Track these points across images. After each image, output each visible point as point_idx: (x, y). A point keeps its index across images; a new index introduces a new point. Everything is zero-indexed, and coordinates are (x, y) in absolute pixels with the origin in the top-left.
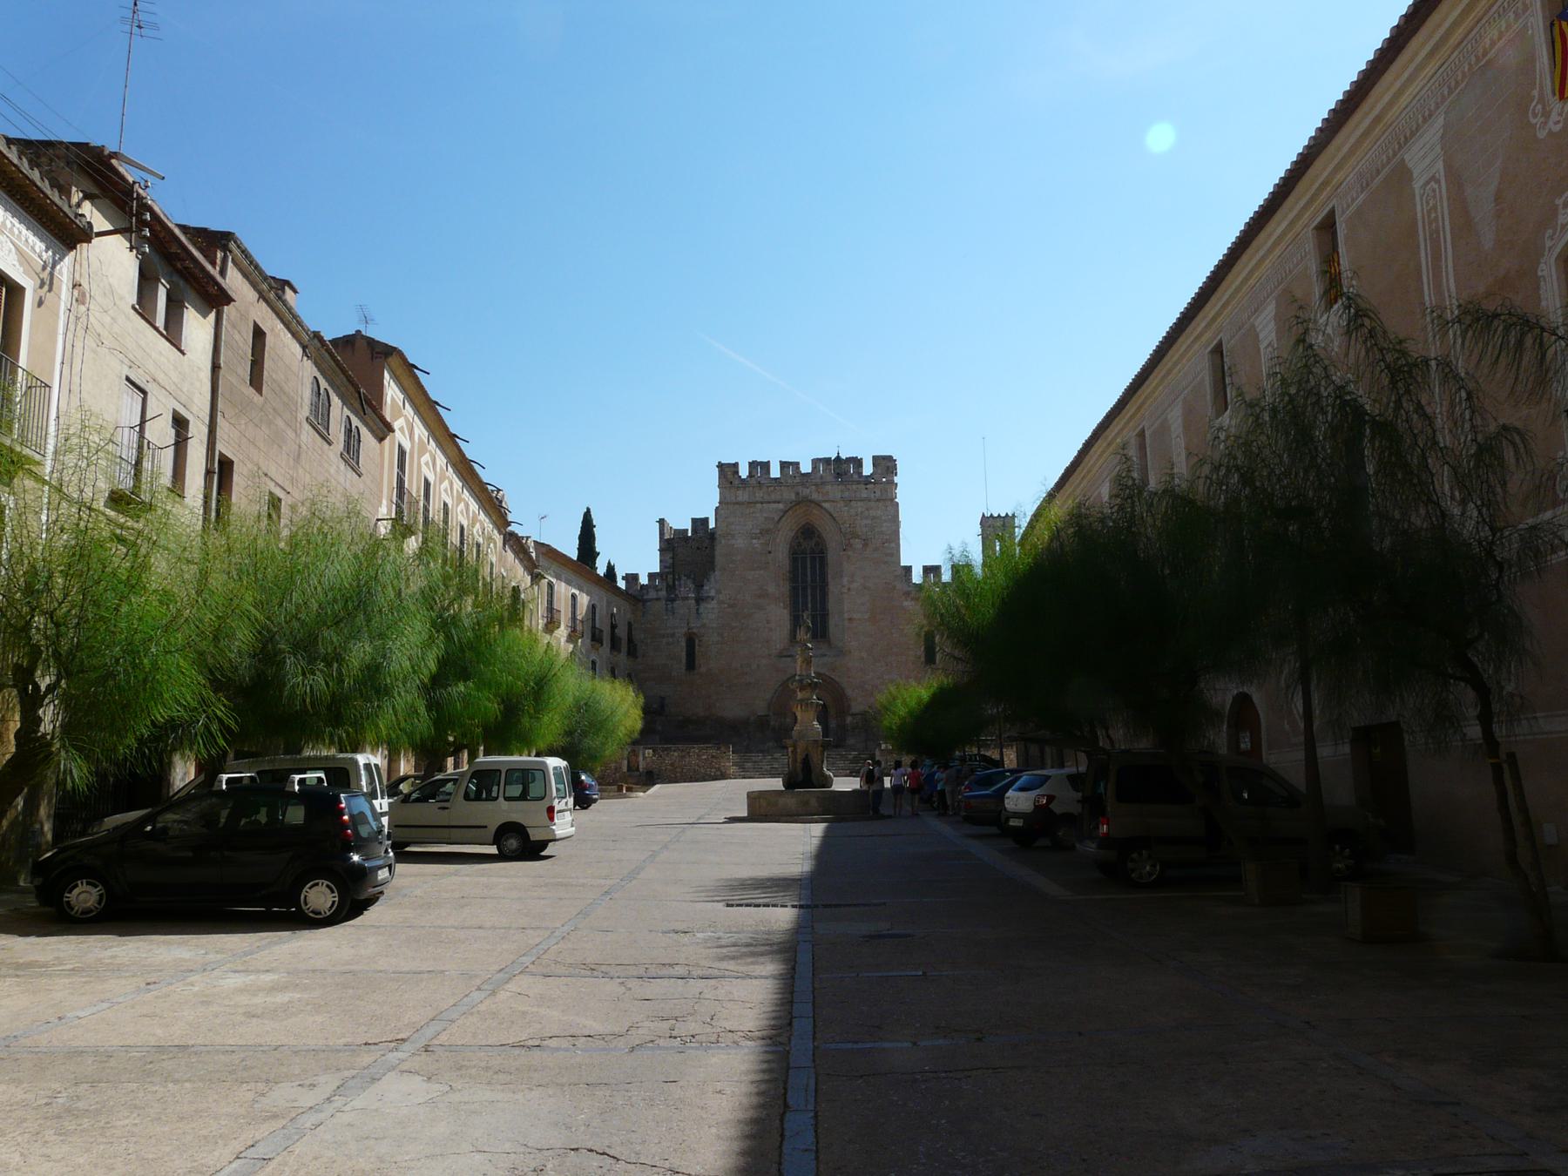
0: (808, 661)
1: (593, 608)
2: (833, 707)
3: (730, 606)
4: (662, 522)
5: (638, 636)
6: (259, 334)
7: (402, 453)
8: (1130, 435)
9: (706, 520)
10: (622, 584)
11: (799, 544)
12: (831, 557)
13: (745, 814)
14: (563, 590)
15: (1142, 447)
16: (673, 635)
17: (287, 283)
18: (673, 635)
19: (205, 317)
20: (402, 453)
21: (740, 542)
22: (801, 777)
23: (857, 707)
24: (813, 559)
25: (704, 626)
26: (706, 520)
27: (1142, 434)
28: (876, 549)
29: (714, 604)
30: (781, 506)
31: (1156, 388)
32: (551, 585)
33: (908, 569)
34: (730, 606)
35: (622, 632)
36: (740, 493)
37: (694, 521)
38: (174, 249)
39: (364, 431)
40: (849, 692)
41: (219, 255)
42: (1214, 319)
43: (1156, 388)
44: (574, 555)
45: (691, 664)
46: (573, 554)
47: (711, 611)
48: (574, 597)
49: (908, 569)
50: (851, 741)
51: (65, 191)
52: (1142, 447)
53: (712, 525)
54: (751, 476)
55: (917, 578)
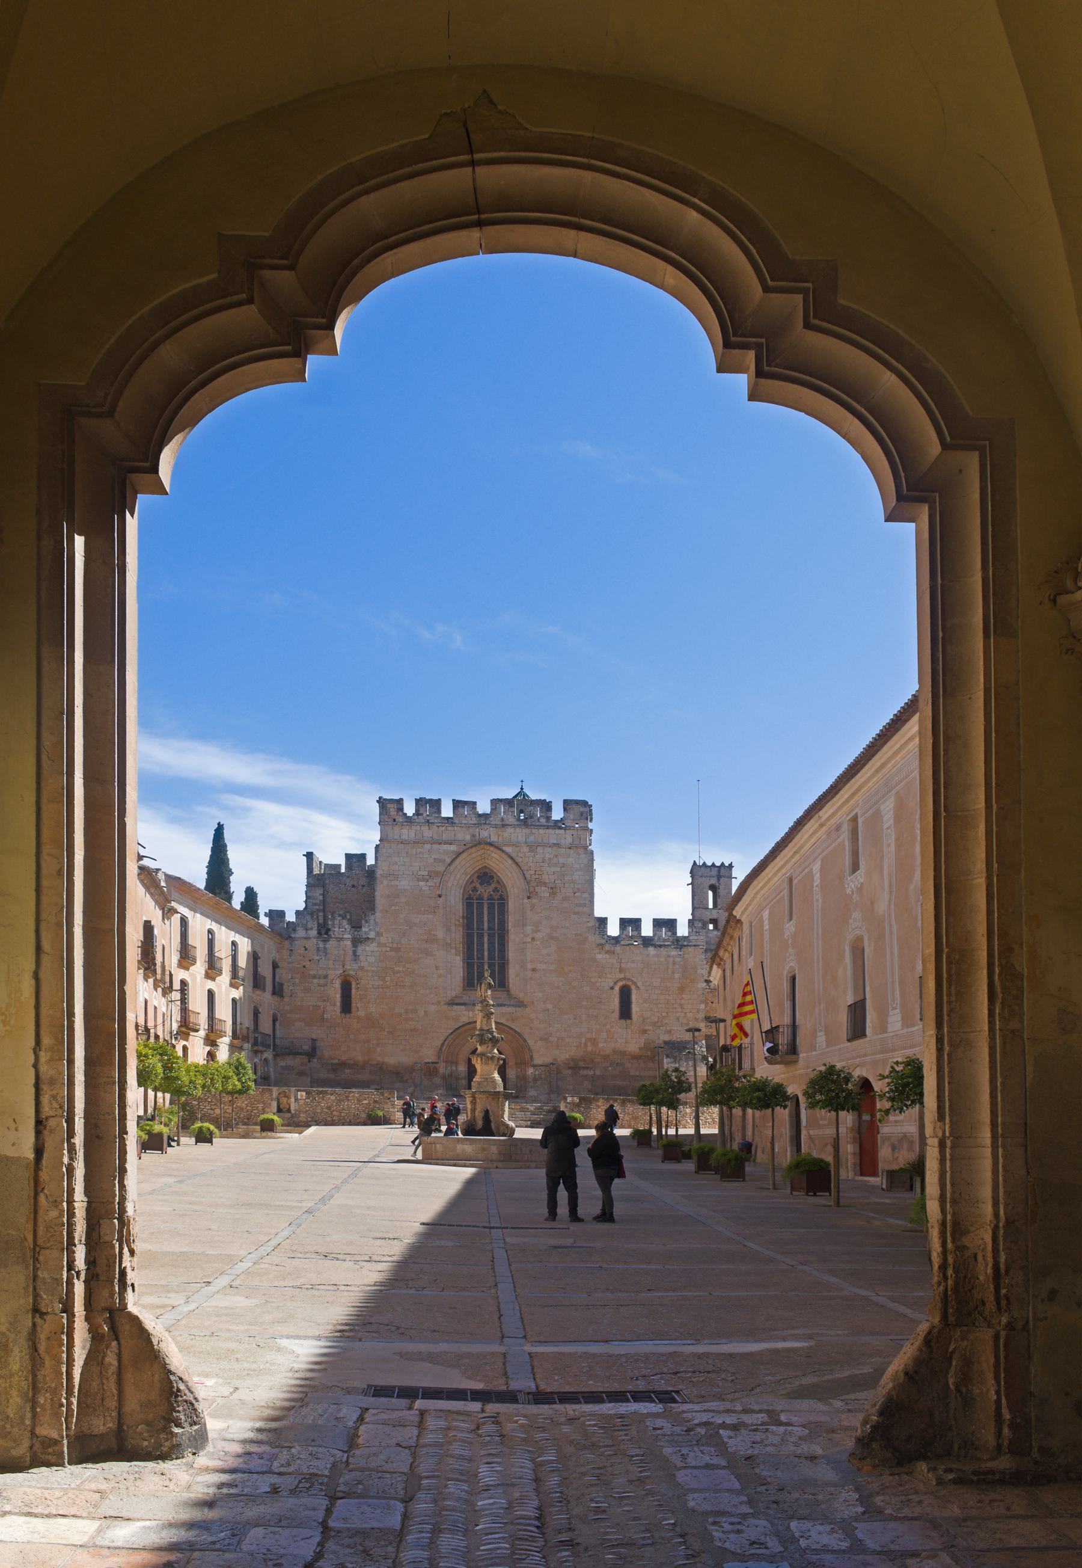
0: (488, 1016)
2: (515, 1058)
3: (392, 949)
4: (309, 856)
5: (283, 974)
8: (843, 817)
9: (362, 857)
10: (264, 921)
11: (475, 890)
12: (512, 905)
14: (200, 924)
15: (854, 833)
16: (326, 977)
18: (326, 977)
21: (404, 884)
22: (480, 1124)
23: (542, 1056)
24: (491, 907)
25: (362, 968)
26: (362, 857)
27: (855, 819)
28: (565, 899)
29: (371, 947)
30: (453, 848)
31: (869, 779)
32: (184, 922)
33: (603, 922)
34: (392, 949)
35: (265, 970)
36: (405, 831)
37: (349, 857)
40: (531, 1043)
42: (883, 766)
43: (869, 779)
44: (201, 884)
45: (347, 1006)
46: (199, 877)
47: (368, 951)
49: (603, 922)
50: (532, 1093)
52: (854, 833)
53: (370, 861)
54: (418, 813)
55: (613, 930)
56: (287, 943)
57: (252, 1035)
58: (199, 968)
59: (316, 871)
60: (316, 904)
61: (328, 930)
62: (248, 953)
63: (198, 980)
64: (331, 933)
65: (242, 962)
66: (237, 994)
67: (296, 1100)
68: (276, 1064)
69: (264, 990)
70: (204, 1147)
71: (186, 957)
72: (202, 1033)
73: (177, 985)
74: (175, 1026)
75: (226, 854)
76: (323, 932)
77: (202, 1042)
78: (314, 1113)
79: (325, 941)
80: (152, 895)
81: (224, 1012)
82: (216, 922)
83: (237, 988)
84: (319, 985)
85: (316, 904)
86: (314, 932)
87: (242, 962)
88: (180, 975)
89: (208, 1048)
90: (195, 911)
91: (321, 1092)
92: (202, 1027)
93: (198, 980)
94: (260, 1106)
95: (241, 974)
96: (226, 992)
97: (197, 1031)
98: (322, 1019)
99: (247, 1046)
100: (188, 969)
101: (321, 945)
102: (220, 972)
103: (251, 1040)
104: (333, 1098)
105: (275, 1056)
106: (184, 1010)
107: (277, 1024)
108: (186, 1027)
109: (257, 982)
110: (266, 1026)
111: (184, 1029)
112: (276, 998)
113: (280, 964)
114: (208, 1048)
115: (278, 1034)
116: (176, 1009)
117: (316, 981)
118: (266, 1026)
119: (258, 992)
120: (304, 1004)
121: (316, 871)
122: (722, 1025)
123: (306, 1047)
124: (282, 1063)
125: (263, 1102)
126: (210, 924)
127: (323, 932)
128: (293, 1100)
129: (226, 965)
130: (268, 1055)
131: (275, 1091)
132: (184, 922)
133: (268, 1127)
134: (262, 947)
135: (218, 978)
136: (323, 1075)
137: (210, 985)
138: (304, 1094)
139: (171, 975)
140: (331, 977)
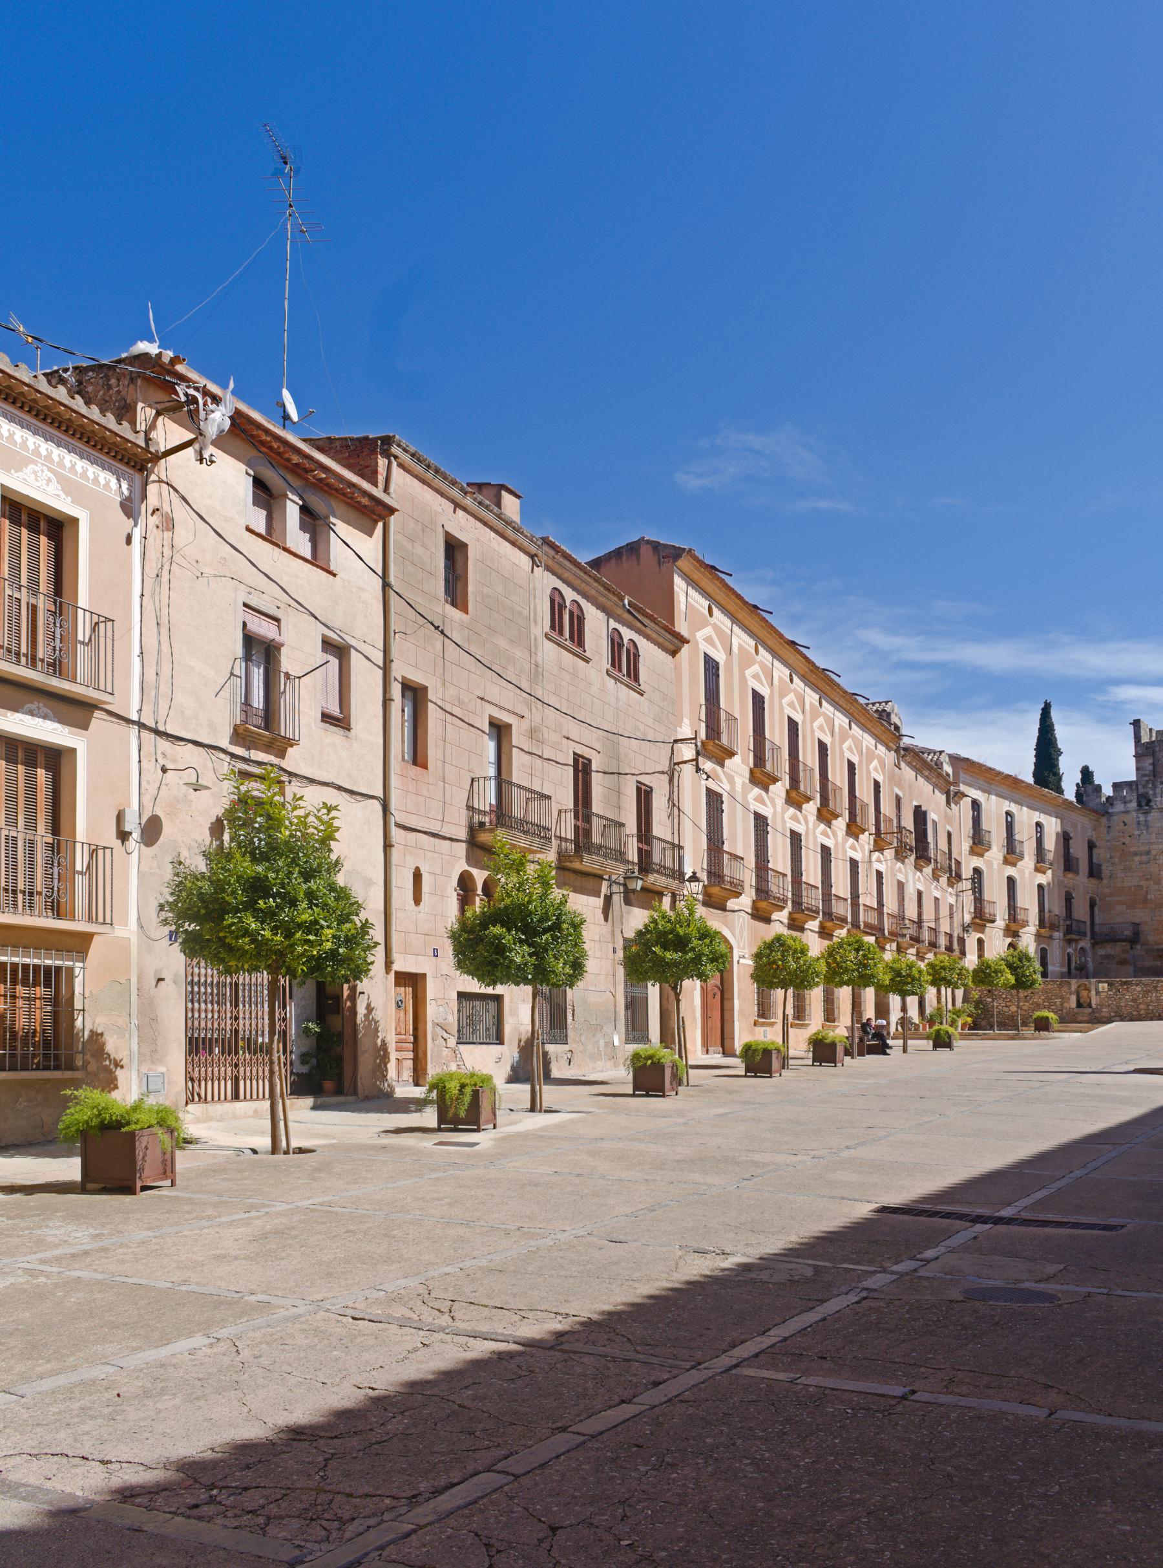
1: (1065, 838)
5: (1100, 854)
6: (454, 549)
7: (711, 667)
13: (97, 714)
14: (1026, 818)
16: (1148, 853)
17: (503, 487)
18: (1148, 853)
19: (370, 534)
20: (711, 667)
32: (976, 805)
35: (1079, 851)
38: (296, 459)
39: (642, 642)
41: (382, 462)
48: (1038, 824)
51: (126, 412)
56: (1104, 820)
57: (1066, 922)
58: (996, 853)
59: (1145, 739)
60: (1145, 775)
61: (1149, 801)
62: (1057, 834)
63: (995, 866)
64: (1152, 804)
65: (1050, 844)
66: (1044, 879)
67: (1098, 993)
68: (1095, 954)
69: (1077, 872)
70: (943, 1053)
71: (979, 842)
72: (1000, 923)
73: (967, 873)
74: (968, 918)
75: (1053, 734)
76: (1144, 803)
77: (1001, 933)
78: (1118, 1007)
79: (1146, 813)
80: (927, 778)
81: (1028, 901)
82: (1016, 802)
83: (1044, 873)
84: (1141, 863)
85: (1145, 775)
86: (1134, 805)
87: (1050, 844)
88: (969, 864)
89: (1009, 940)
90: (989, 793)
91: (1125, 983)
92: (998, 918)
93: (995, 866)
94: (1058, 1001)
95: (1050, 856)
96: (1030, 877)
97: (993, 922)
98: (1146, 901)
99: (1056, 935)
100: (982, 856)
101: (1142, 819)
102: (1022, 857)
103: (1062, 929)
104: (1138, 988)
105: (1094, 945)
106: (979, 900)
107: (1096, 909)
108: (981, 919)
109: (1069, 864)
110: (1081, 911)
111: (977, 921)
112: (1093, 880)
113: (1097, 844)
114: (1009, 940)
115: (1097, 920)
116: (968, 899)
117: (1137, 858)
118: (1081, 911)
119: (1070, 875)
120: (1125, 885)
121: (1145, 739)
122: (109, 624)
123: (1128, 933)
124: (1102, 952)
125: (1062, 997)
126: (1008, 806)
127: (1144, 803)
128: (1093, 992)
129: (1029, 850)
130: (1085, 943)
131: (1074, 982)
132: (976, 805)
133: (1043, 1025)
134: (1074, 825)
135: (1019, 864)
136: (1149, 963)
137: (1010, 871)
138: (1106, 985)
139: (958, 863)
140: (1154, 853)
